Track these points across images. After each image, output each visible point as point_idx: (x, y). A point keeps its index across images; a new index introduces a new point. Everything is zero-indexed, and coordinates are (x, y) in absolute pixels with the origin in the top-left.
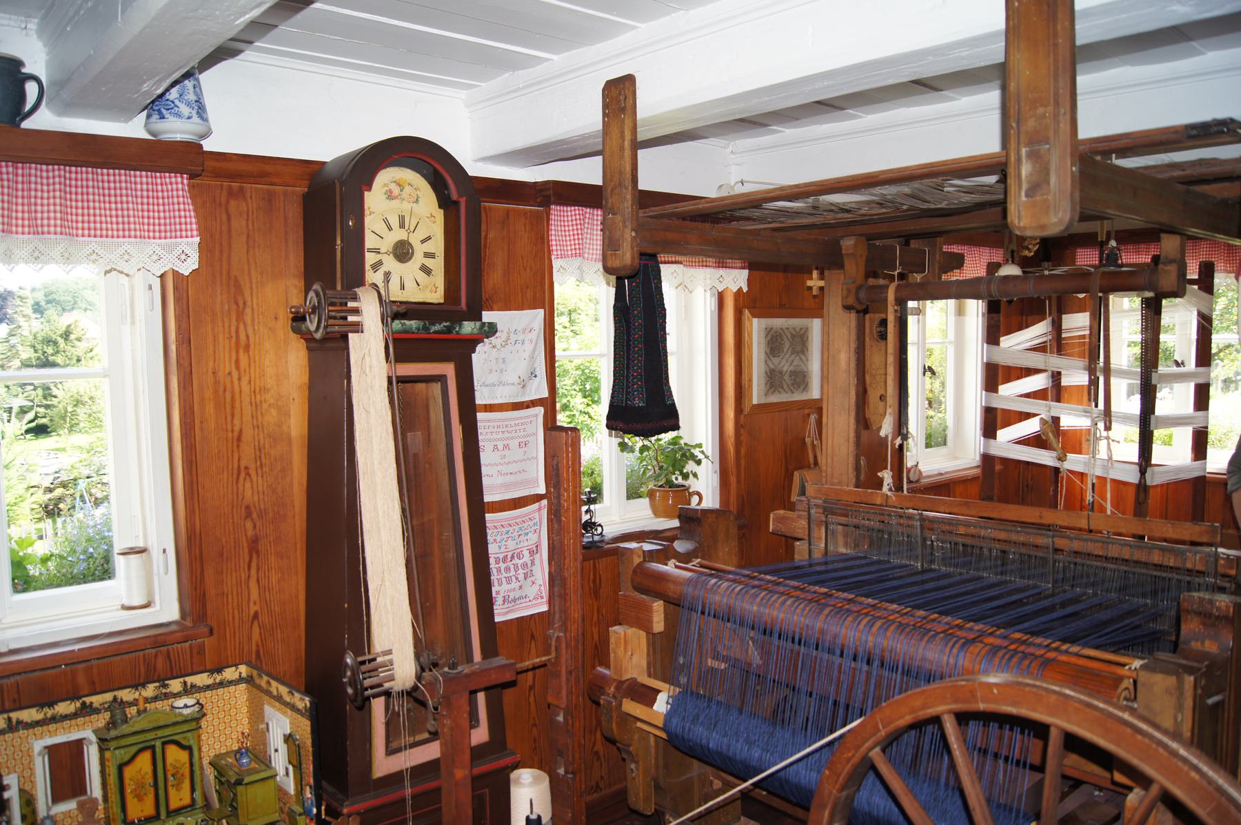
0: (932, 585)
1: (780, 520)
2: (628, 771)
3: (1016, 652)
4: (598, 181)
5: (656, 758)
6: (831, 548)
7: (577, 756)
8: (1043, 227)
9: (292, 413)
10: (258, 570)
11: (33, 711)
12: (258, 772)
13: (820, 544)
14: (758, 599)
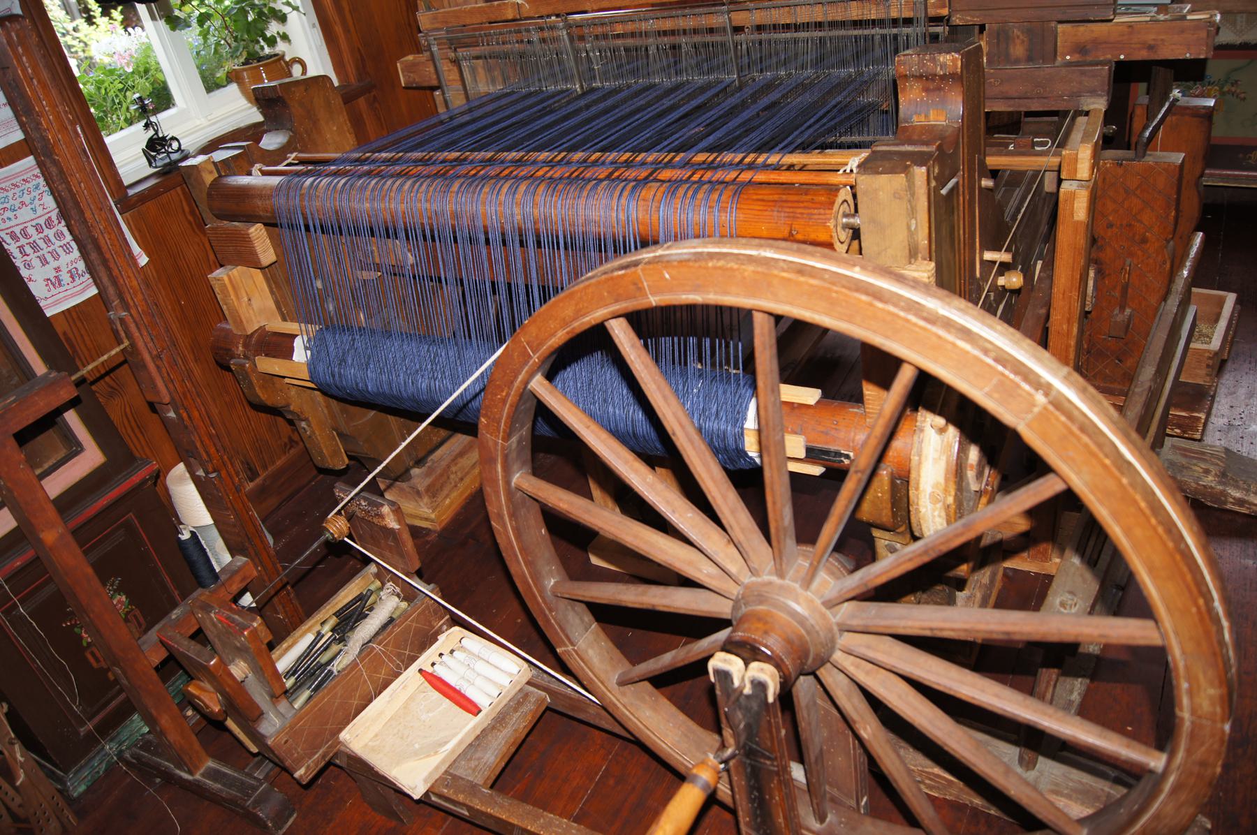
1: (410, 68)
2: (301, 431)
3: (700, 182)
7: (212, 450)
13: (467, 84)
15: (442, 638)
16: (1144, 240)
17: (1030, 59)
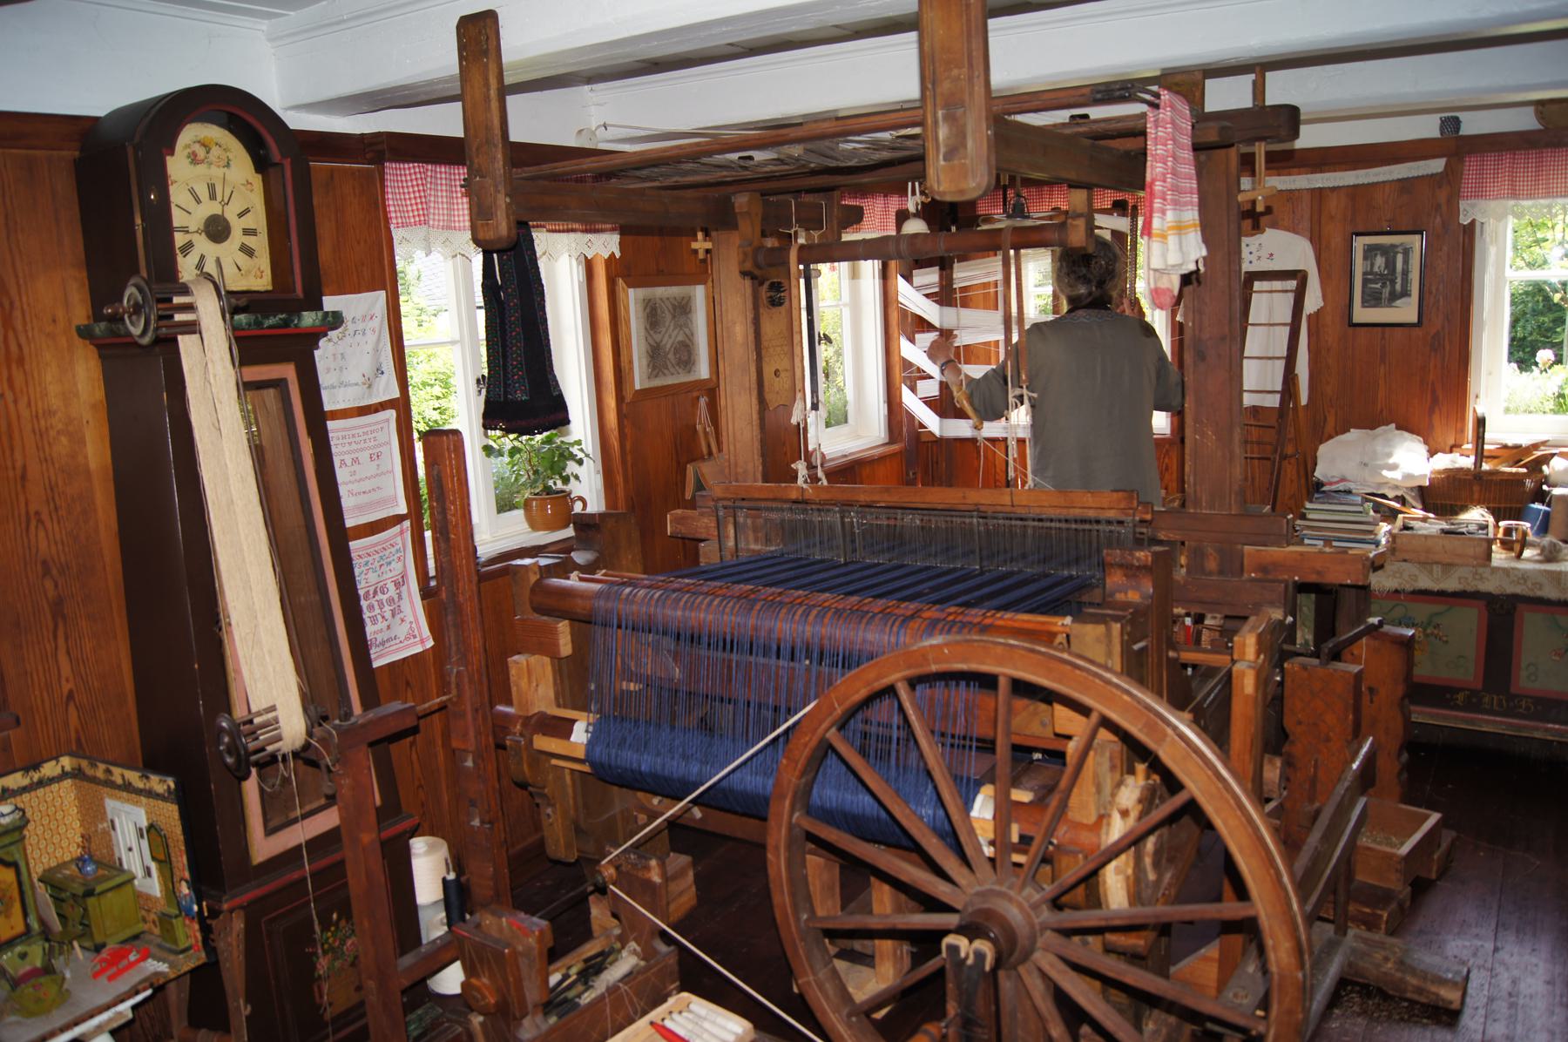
0: (858, 575)
2: (544, 817)
4: (458, 132)
5: (575, 798)
6: (742, 545)
8: (962, 192)
9: (88, 439)
10: (67, 639)
11: (18, 775)
12: (109, 878)
13: (731, 540)
15: (671, 1001)
16: (1328, 740)
17: (1221, 572)
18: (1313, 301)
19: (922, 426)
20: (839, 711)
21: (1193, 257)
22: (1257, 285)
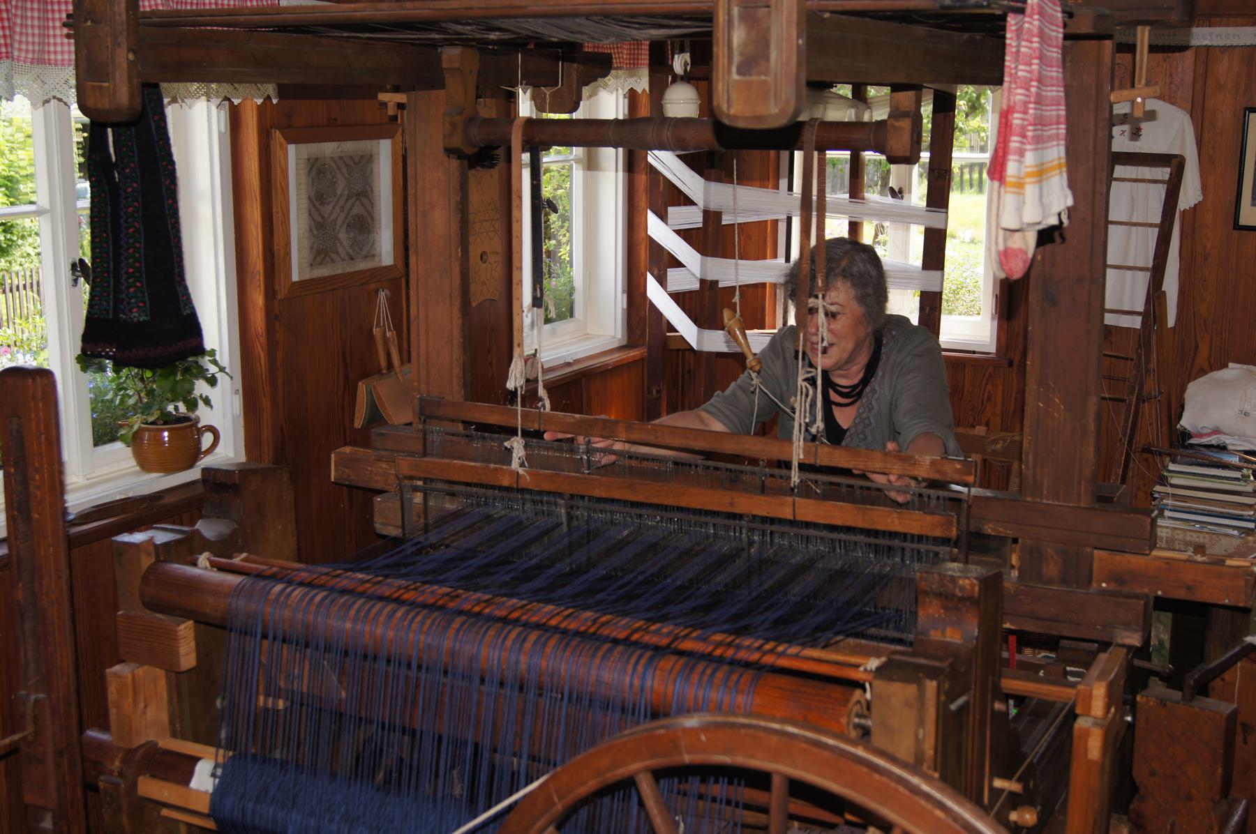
1: (344, 462)
8: (760, 118)
14: (352, 612)
16: (1189, 798)
17: (1063, 581)
18: (1190, 194)
19: (672, 328)
20: (559, 807)
21: (1056, 210)
22: (1120, 171)
